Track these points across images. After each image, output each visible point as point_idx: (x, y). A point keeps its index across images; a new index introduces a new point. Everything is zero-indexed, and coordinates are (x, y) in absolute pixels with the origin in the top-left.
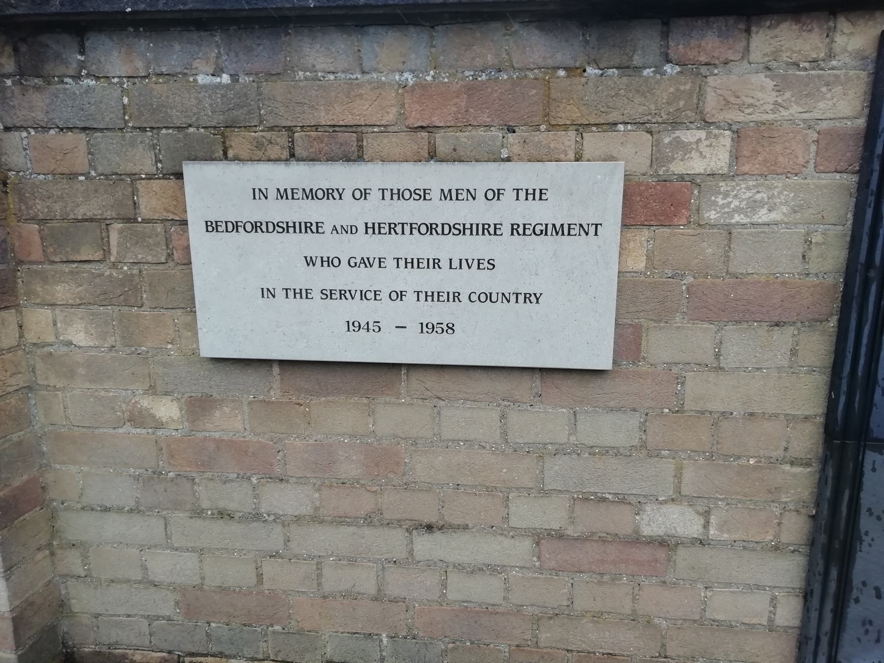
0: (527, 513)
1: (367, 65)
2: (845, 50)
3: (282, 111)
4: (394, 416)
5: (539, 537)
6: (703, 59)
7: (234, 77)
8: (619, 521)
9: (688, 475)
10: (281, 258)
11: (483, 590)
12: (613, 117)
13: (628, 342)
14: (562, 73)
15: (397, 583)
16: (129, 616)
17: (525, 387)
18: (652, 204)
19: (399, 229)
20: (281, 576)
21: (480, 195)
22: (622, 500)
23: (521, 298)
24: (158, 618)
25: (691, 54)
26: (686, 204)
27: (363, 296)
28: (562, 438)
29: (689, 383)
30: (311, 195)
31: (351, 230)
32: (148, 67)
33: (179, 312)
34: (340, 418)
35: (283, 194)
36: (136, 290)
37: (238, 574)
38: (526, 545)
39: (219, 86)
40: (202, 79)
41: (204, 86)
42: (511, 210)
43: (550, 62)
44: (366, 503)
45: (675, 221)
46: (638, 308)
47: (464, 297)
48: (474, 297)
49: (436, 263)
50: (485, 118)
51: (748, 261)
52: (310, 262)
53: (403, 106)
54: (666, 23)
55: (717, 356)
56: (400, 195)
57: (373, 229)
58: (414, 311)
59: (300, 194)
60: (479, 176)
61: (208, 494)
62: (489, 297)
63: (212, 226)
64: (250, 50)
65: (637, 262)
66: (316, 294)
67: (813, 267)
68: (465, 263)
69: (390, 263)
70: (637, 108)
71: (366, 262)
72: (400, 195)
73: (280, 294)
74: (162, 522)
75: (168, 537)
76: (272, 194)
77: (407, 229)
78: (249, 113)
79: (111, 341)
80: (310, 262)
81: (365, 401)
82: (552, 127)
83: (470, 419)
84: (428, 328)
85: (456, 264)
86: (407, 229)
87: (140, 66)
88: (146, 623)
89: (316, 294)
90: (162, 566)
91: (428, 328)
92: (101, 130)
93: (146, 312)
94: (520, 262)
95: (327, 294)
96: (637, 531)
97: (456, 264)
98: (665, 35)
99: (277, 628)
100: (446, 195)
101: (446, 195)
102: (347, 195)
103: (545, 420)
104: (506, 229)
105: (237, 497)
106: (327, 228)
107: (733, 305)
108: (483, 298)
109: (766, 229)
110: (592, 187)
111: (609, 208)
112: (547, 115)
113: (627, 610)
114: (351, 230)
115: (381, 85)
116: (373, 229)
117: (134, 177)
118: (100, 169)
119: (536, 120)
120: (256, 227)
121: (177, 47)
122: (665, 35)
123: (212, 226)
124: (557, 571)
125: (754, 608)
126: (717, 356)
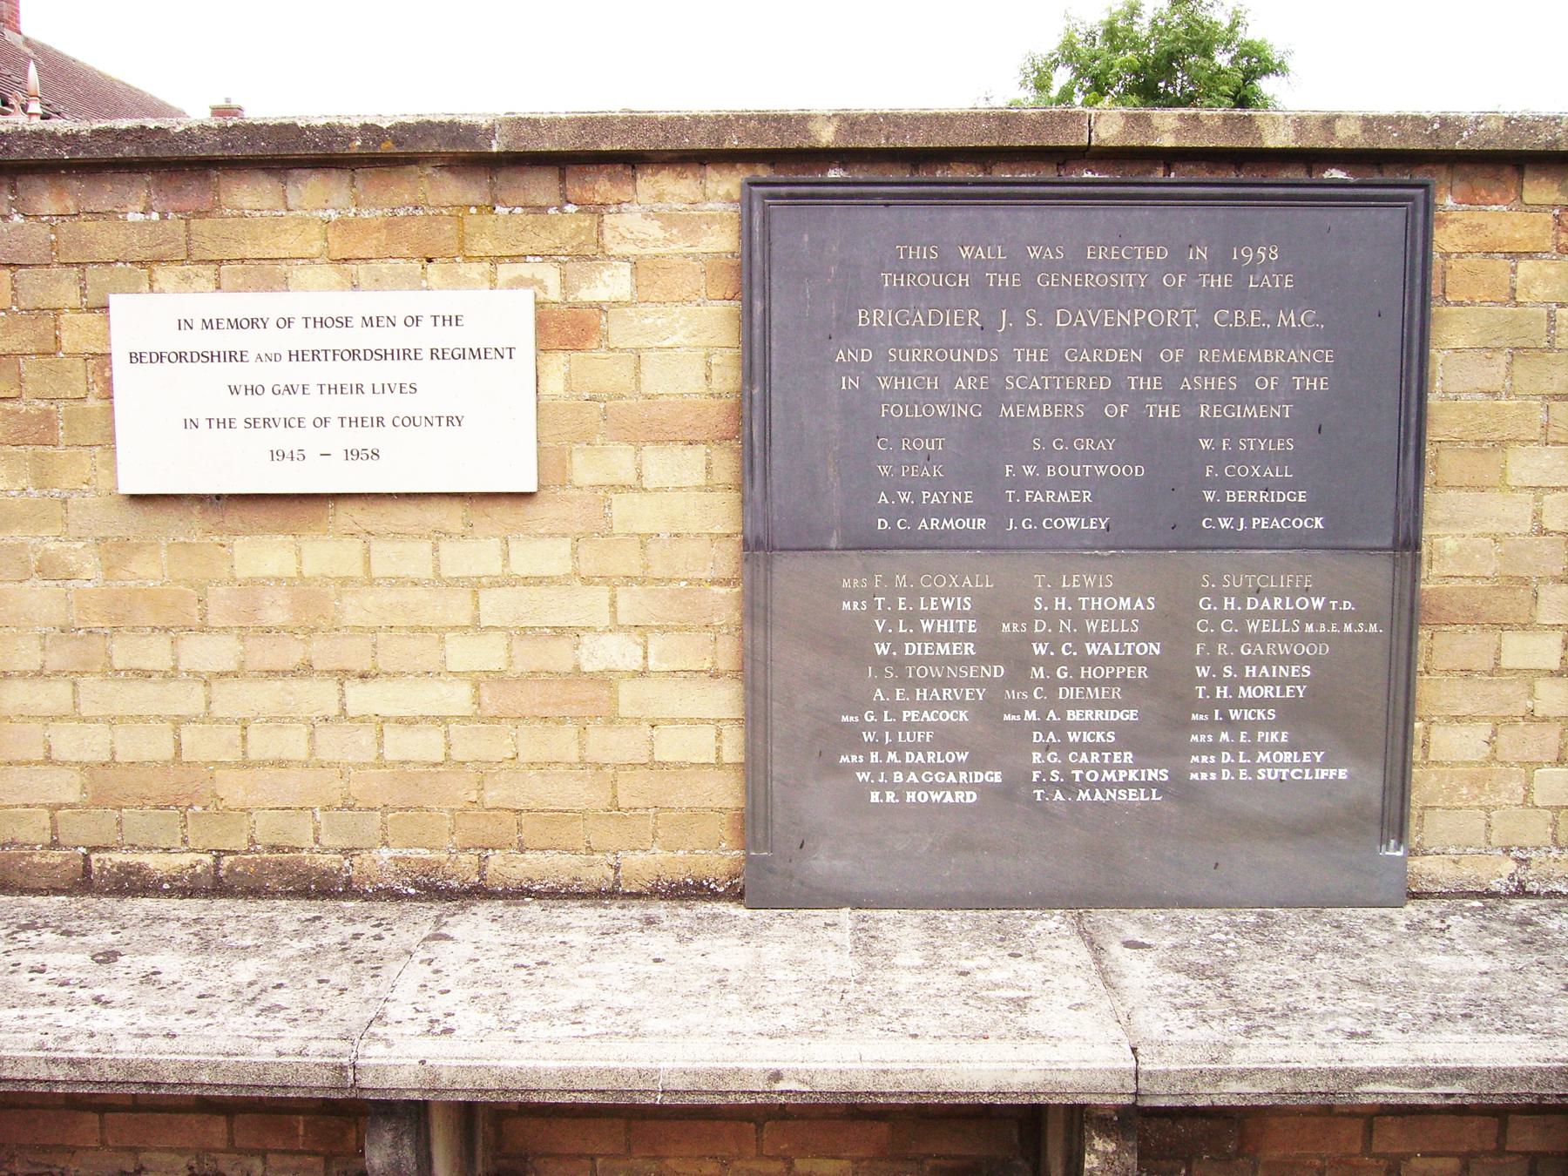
0: (466, 654)
1: (292, 203)
2: (716, 194)
3: (209, 246)
4: (323, 552)
5: (479, 680)
6: (598, 199)
7: (163, 216)
8: (559, 656)
9: (622, 603)
10: (206, 387)
11: (424, 746)
12: (523, 249)
13: (551, 461)
14: (473, 210)
15: (332, 744)
16: (27, 806)
17: (452, 516)
18: (563, 329)
19: (322, 356)
20: (202, 745)
21: (400, 322)
22: (559, 632)
23: (444, 421)
24: (59, 807)
25: (588, 195)
26: (596, 328)
27: (287, 424)
28: (496, 569)
29: (615, 505)
30: (236, 324)
31: (276, 358)
32: (77, 206)
33: (98, 449)
34: (265, 554)
35: (208, 324)
36: (52, 427)
37: (154, 746)
38: (464, 691)
39: (149, 223)
40: (131, 217)
41: (133, 223)
42: (426, 337)
43: (462, 201)
44: (293, 654)
45: (588, 344)
46: (556, 433)
47: (388, 422)
48: (398, 422)
49: (359, 388)
50: (405, 251)
51: (657, 379)
52: (234, 390)
53: (326, 240)
54: (562, 170)
55: (640, 476)
56: (323, 323)
57: (298, 356)
58: (340, 438)
59: (225, 323)
60: (397, 302)
61: (123, 653)
62: (412, 421)
63: (136, 358)
64: (180, 189)
65: (554, 385)
66: (239, 423)
67: (717, 386)
68: (387, 388)
69: (313, 389)
70: (544, 242)
71: (290, 390)
72: (323, 323)
73: (204, 424)
74: (70, 687)
75: (76, 705)
76: (198, 324)
77: (330, 355)
78: (177, 247)
79: (23, 482)
80: (234, 390)
81: (291, 538)
82: (468, 259)
83: (402, 553)
84: (353, 454)
85: (378, 389)
86: (330, 355)
87: (70, 205)
88: (47, 814)
89: (239, 423)
90: (67, 742)
91: (353, 454)
92: (26, 266)
93: (60, 450)
94: (440, 386)
95: (252, 423)
96: (577, 668)
97: (378, 389)
98: (562, 179)
99: (198, 809)
100: (367, 322)
101: (367, 322)
102: (271, 324)
103: (476, 551)
104: (426, 354)
105: (156, 653)
106: (251, 356)
107: (653, 430)
108: (406, 422)
109: (670, 352)
110: (500, 310)
111: (523, 335)
112: (462, 248)
113: (573, 756)
114: (276, 358)
115: (305, 221)
116: (298, 356)
117: (57, 310)
118: (23, 304)
119: (454, 251)
120: (180, 357)
121: (109, 188)
122: (562, 179)
123: (136, 358)
124: (496, 719)
125: (696, 745)
126: (640, 476)
